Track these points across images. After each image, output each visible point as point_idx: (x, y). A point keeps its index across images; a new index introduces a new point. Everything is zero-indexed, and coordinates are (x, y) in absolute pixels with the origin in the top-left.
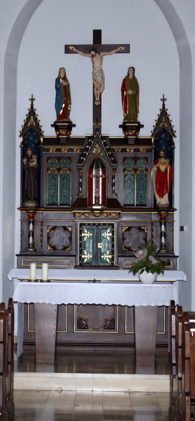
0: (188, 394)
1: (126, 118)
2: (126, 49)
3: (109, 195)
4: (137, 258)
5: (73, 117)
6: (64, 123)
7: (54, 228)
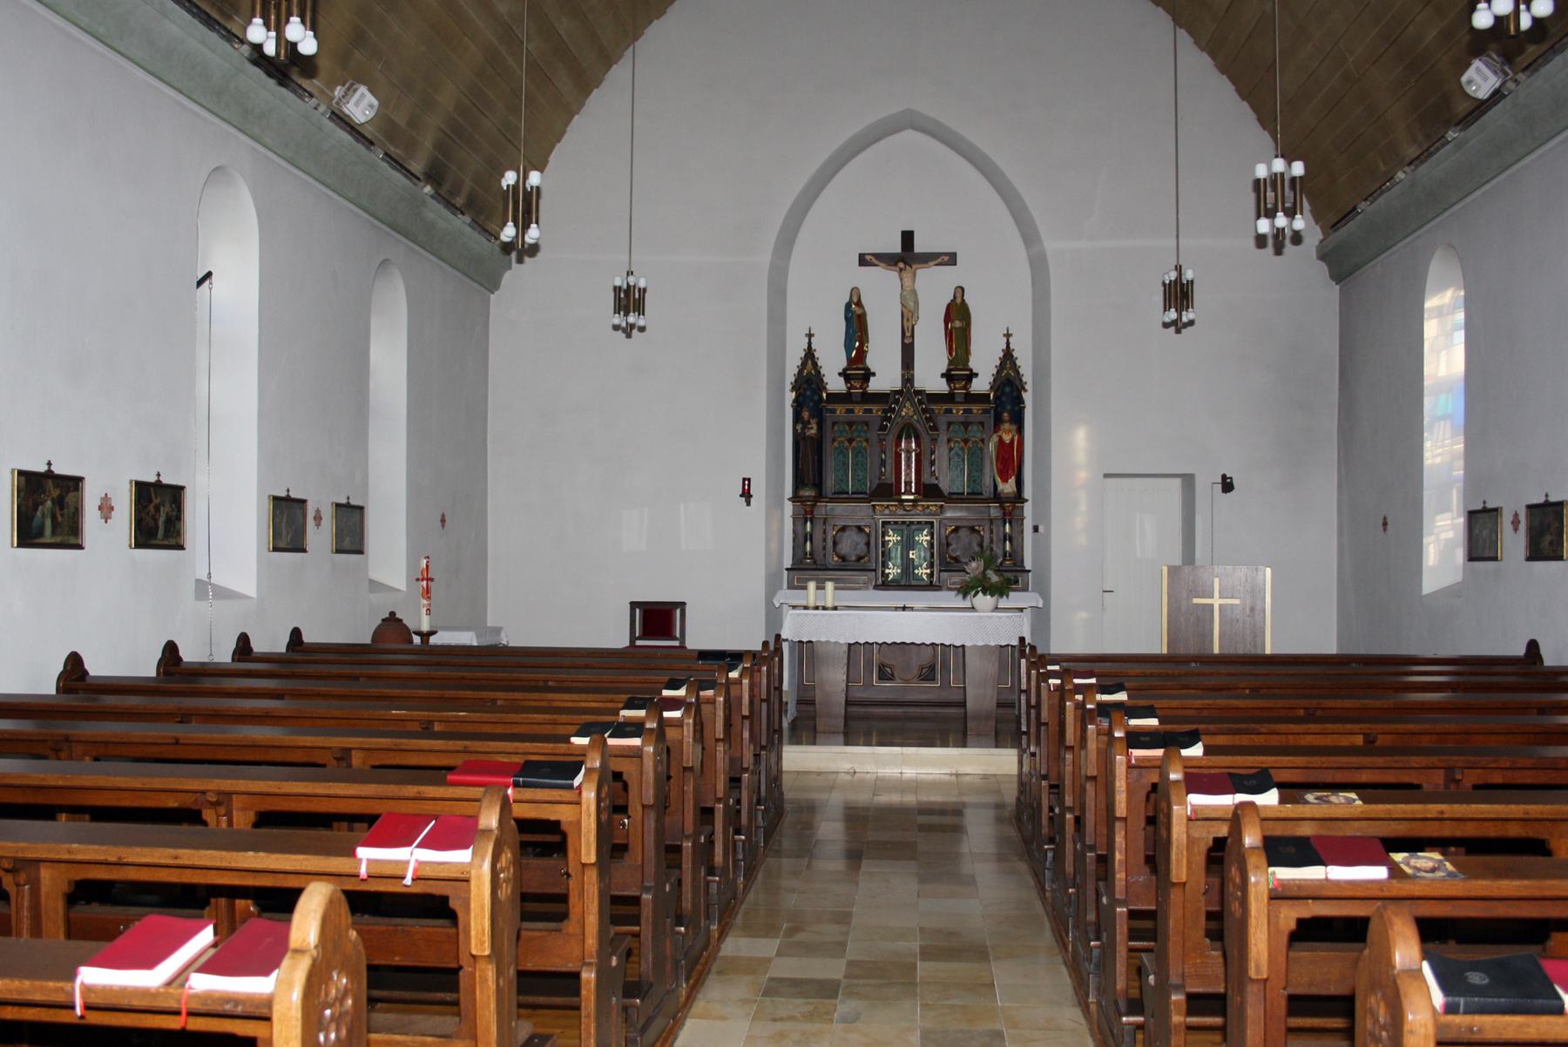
0: (1045, 777)
1: (951, 362)
2: (951, 259)
3: (926, 479)
5: (871, 362)
6: (857, 370)
7: (843, 529)
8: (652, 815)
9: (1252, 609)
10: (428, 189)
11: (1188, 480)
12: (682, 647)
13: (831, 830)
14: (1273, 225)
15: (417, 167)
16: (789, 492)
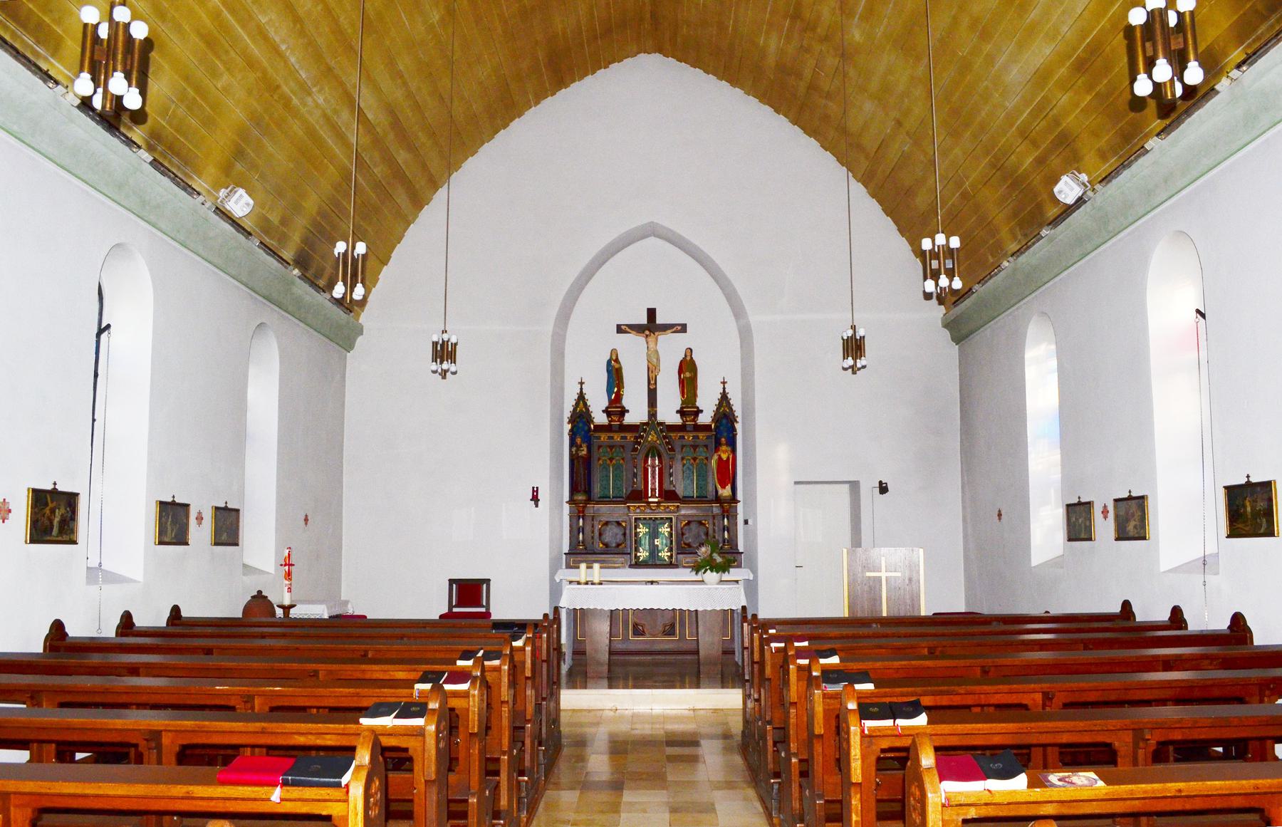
0: (769, 723)
2: (683, 328)
3: (666, 486)
4: (199, 194)
5: (626, 402)
6: (616, 408)
7: (607, 523)
8: (434, 790)
9: (910, 580)
10: (296, 272)
11: (854, 486)
12: (488, 614)
13: (599, 764)
14: (937, 285)
15: (288, 255)
16: (566, 498)
